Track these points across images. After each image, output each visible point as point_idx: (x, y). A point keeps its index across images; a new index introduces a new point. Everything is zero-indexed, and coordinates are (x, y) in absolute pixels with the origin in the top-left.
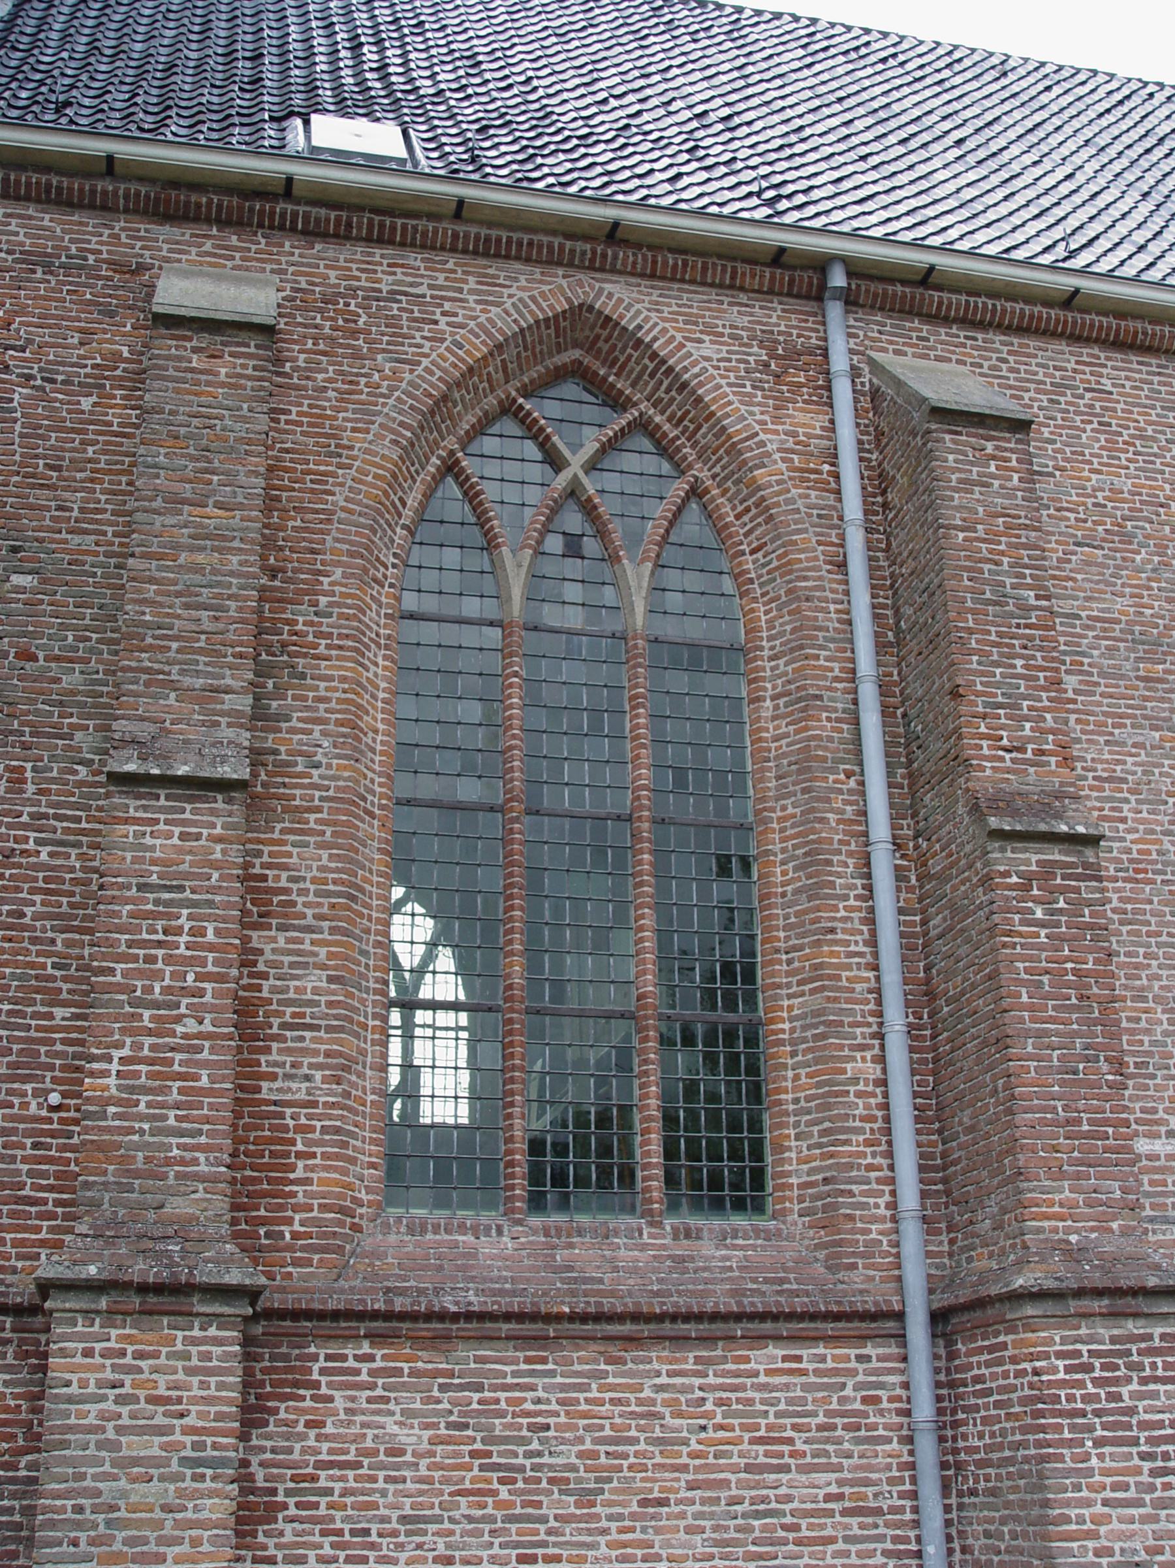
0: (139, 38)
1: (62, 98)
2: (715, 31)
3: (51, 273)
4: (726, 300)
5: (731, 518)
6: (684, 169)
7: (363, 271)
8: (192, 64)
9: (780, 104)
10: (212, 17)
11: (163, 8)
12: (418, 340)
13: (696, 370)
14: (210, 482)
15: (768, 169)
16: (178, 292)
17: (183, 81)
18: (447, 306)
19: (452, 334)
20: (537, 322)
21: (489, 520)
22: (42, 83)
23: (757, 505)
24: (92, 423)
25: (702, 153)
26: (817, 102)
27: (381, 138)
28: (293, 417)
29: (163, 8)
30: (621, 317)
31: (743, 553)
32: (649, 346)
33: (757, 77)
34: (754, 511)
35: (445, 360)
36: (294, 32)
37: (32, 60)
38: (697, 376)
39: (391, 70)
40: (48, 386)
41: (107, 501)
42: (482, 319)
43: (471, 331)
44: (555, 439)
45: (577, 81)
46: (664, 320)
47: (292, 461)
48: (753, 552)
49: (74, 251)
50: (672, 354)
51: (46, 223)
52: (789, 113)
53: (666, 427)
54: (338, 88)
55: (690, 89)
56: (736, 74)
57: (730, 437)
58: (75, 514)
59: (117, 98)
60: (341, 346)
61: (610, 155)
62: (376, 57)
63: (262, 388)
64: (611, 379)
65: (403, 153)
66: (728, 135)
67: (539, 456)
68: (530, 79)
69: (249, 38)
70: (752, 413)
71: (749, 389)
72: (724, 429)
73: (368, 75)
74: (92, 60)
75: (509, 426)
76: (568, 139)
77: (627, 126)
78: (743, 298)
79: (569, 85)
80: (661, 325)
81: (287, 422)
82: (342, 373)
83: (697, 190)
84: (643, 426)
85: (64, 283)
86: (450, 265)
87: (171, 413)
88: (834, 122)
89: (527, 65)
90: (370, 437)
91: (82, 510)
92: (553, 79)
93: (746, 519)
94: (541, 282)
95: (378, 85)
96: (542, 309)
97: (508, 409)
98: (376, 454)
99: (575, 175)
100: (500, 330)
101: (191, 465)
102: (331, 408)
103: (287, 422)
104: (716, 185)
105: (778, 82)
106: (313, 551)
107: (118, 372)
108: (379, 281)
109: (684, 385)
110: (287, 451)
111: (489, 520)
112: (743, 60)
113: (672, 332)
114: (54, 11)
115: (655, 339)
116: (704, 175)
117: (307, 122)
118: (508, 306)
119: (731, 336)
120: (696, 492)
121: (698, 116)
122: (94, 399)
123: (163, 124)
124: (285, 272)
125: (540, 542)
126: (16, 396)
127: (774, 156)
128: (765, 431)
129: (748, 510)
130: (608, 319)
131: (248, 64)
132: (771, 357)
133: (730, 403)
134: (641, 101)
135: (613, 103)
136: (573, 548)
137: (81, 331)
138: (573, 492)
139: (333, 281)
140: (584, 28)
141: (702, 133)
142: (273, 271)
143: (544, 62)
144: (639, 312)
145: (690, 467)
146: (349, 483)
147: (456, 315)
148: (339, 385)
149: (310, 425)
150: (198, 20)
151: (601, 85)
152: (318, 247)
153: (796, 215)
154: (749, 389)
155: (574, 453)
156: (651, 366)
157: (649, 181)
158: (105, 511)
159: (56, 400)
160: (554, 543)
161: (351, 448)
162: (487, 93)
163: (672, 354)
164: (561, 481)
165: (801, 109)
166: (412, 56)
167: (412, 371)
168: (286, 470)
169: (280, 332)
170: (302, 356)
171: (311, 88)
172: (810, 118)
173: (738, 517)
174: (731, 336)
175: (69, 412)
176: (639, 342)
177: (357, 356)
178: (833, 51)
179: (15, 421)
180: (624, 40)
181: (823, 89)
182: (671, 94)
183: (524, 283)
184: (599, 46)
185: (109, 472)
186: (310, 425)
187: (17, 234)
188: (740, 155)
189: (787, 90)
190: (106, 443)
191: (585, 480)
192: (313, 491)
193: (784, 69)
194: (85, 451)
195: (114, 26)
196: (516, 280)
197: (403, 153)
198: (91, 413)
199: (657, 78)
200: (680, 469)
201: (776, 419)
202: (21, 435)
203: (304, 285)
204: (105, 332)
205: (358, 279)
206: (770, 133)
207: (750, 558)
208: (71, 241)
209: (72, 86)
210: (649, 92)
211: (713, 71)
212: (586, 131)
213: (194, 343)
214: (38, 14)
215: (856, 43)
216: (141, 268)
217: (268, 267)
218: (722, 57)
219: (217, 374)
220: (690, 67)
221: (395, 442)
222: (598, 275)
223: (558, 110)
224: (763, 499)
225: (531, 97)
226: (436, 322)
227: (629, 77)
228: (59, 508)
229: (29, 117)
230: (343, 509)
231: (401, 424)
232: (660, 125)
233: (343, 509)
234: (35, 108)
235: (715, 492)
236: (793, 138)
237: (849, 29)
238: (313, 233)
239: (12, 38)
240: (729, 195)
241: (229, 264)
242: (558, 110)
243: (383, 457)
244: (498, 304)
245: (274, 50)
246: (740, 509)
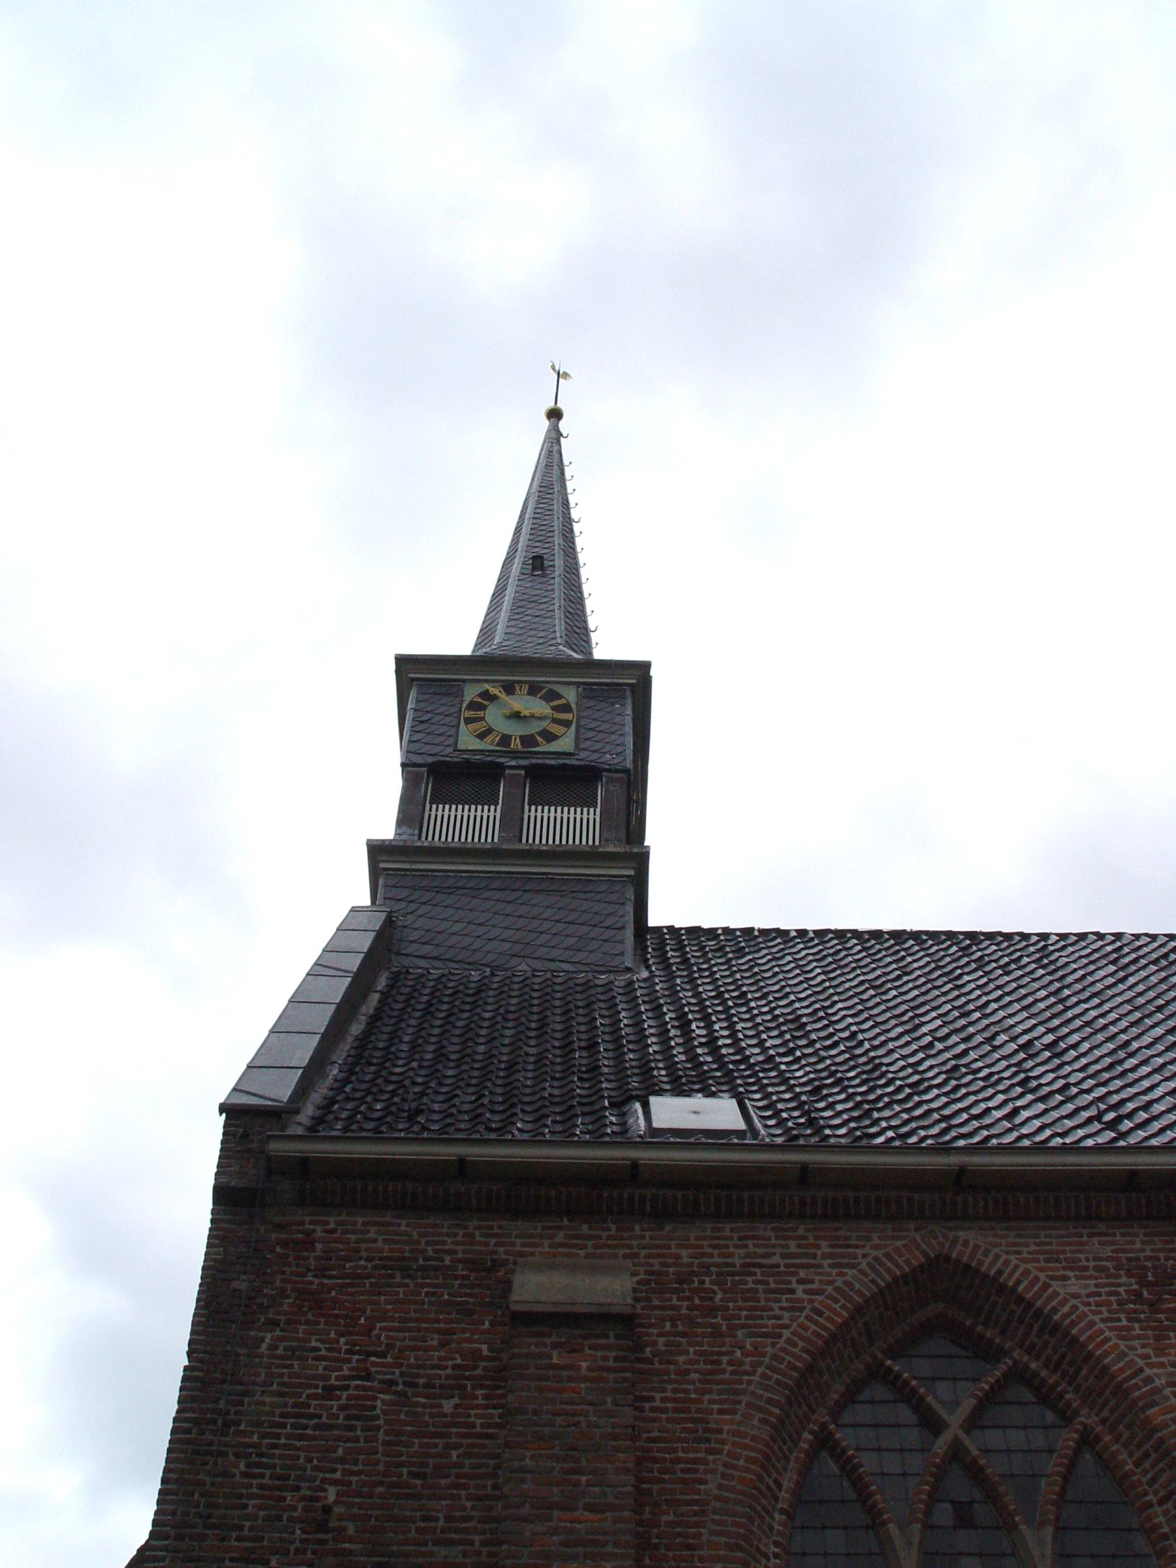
0: (482, 1040)
1: (414, 1105)
2: (1026, 960)
3: (410, 1277)
4: (1085, 1232)
5: (1129, 1467)
6: (1019, 1103)
7: (715, 1247)
8: (531, 1059)
9: (1102, 1021)
10: (548, 1013)
11: (502, 1011)
12: (777, 1312)
13: (1066, 1309)
14: (577, 1484)
15: (1103, 1090)
16: (535, 1287)
17: (526, 1077)
18: (802, 1273)
19: (811, 1301)
20: (895, 1279)
21: (871, 1494)
22: (394, 1093)
23: (1156, 1448)
24: (455, 1425)
25: (1034, 1083)
26: (1138, 1015)
27: (720, 1113)
28: (657, 1403)
29: (502, 1011)
30: (980, 1263)
31: (1150, 1505)
32: (1013, 1290)
33: (1074, 999)
34: (1154, 1455)
35: (806, 1329)
36: (625, 1018)
37: (384, 1073)
38: (1068, 1315)
39: (720, 1043)
40: (410, 1391)
41: (473, 1508)
42: (839, 1283)
43: (830, 1297)
44: (929, 1399)
45: (900, 1030)
46: (1023, 1260)
47: (660, 1450)
48: (1161, 1502)
49: (430, 1253)
50: (1038, 1295)
51: (403, 1228)
52: (1114, 1029)
53: (1044, 1373)
54: (671, 1067)
55: (1011, 1022)
56: (1053, 1000)
57: (1113, 1377)
58: (441, 1523)
59: (465, 1099)
60: (700, 1325)
61: (944, 1099)
62: (704, 1032)
63: (625, 1380)
64: (979, 1328)
65: (741, 1125)
66: (1057, 1061)
67: (914, 1419)
68: (854, 1034)
69: (583, 1028)
70: (1132, 1348)
71: (1124, 1323)
72: (1106, 1368)
73: (699, 1051)
74: (440, 1066)
75: (880, 1391)
76: (899, 1089)
77: (956, 1068)
78: (1101, 1227)
79: (892, 1034)
80: (1023, 1266)
81: (652, 1409)
82: (702, 1353)
83: (1037, 1123)
84: (1019, 1374)
85: (423, 1286)
86: (800, 1232)
87: (535, 1413)
88: (1159, 1031)
89: (850, 1020)
90: (738, 1417)
91: (448, 1519)
92: (877, 1030)
93: (1147, 1465)
94: (893, 1238)
95: (709, 1059)
96: (898, 1266)
97: (877, 1373)
98: (745, 1435)
99: (914, 1125)
100: (859, 1292)
101: (558, 1467)
102: (696, 1391)
103: (652, 1409)
104: (1055, 1114)
105: (1096, 1001)
106: (690, 1547)
107: (479, 1372)
108: (731, 1255)
109: (1057, 1325)
110: (654, 1440)
111: (871, 1494)
112: (1057, 985)
113: (1034, 1273)
114: (403, 1025)
115: (1019, 1282)
116: (1041, 1106)
117: (646, 1106)
118: (864, 1266)
119: (1096, 1268)
120: (1087, 1440)
121: (1023, 1047)
122: (456, 1400)
123: (508, 1122)
124: (636, 1256)
125: (928, 1513)
126: (379, 1403)
127: (1106, 1075)
128: (1151, 1365)
129: (1146, 1455)
130: (967, 1267)
131: (585, 1054)
132: (1141, 1285)
133: (1107, 1340)
134: (964, 1040)
135: (939, 1046)
136: (964, 1518)
137: (439, 1331)
138: (956, 1452)
139: (686, 1260)
140: (899, 977)
141: (1030, 1063)
142: (625, 1256)
143: (865, 1015)
144: (997, 1256)
145: (1076, 1413)
146: (721, 1469)
147: (811, 1281)
148: (702, 1366)
149: (675, 1410)
150: (535, 1017)
151: (924, 1029)
152: (668, 1227)
153: (1142, 1134)
154: (1124, 1323)
155: (956, 1435)
156: (1018, 1311)
157: (987, 1121)
158: (471, 1518)
159: (417, 1404)
160: (944, 1513)
161: (719, 1431)
162: (815, 1053)
163: (1038, 1295)
164: (941, 1444)
165: (1123, 1024)
166: (739, 1027)
167: (773, 1345)
168: (655, 1460)
169: (637, 1316)
170: (662, 1340)
171: (646, 1070)
172: (1135, 1031)
173: (1137, 1464)
174: (1096, 1268)
175: (431, 1416)
176: (1003, 1287)
177: (717, 1334)
178: (1143, 962)
179: (378, 1428)
180: (939, 983)
181: (1141, 1000)
182: (994, 1029)
183: (876, 1241)
184: (916, 992)
185: (471, 1477)
186: (675, 1410)
187: (375, 1241)
188: (1072, 1080)
189: (1106, 1007)
190: (470, 1446)
191: (967, 1442)
192: (684, 1481)
193: (1099, 986)
194: (448, 1456)
195: (457, 1032)
196: (869, 1239)
197: (741, 1125)
198: (454, 1415)
199: (978, 1015)
200: (1066, 1417)
201: (1160, 1351)
202: (384, 1443)
203: (657, 1267)
204: (464, 1331)
205: (711, 1256)
206: (1098, 1053)
207: (1159, 1510)
208: (427, 1243)
209: (422, 1094)
210: (971, 1030)
211: (1030, 999)
212: (916, 1078)
213: (554, 1339)
214: (389, 1029)
215: (1164, 950)
216: (497, 1264)
217: (621, 1252)
218: (1036, 985)
219: (578, 1368)
220: (1008, 999)
221: (763, 1421)
222: (952, 1224)
223: (885, 1060)
224: (1161, 1442)
225: (858, 1051)
226: (792, 1291)
227: (950, 1018)
228: (425, 1519)
229: (384, 1129)
230: (718, 1498)
231: (770, 1401)
232: (988, 1061)
233: (718, 1498)
234: (389, 1119)
235: (1107, 1438)
236: (1122, 1054)
237: (1154, 937)
238: (661, 1214)
239: (366, 1054)
240: (1069, 1123)
241: (582, 1252)
242: (885, 1060)
243: (754, 1438)
244: (853, 1266)
245: (607, 1037)
246: (1138, 1454)
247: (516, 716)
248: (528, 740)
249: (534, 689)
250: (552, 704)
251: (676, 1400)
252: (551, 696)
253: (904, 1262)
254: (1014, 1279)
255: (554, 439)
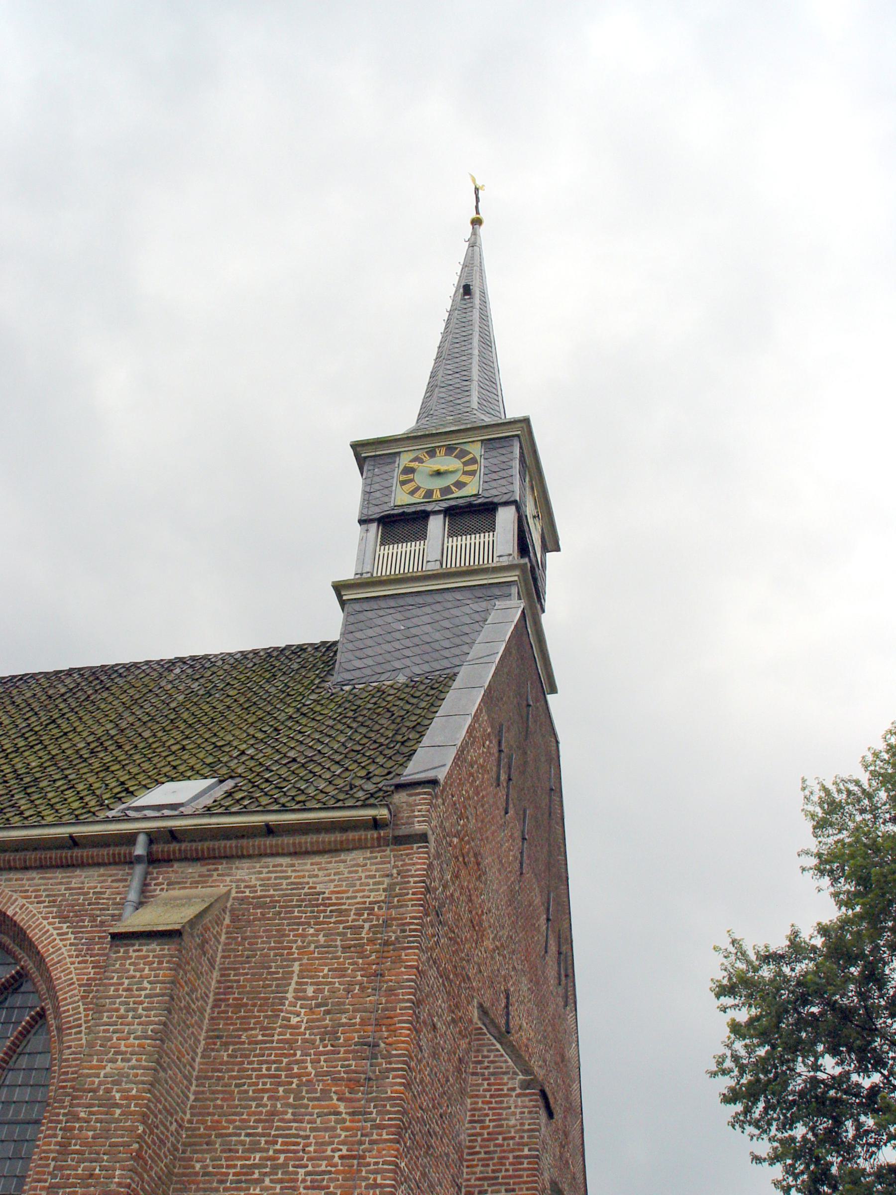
247: (438, 473)
248: (446, 490)
249: (450, 450)
250: (463, 460)
251: (289, 918)
252: (463, 454)
253: (281, 1075)
254: (66, 1008)
255: (473, 244)
